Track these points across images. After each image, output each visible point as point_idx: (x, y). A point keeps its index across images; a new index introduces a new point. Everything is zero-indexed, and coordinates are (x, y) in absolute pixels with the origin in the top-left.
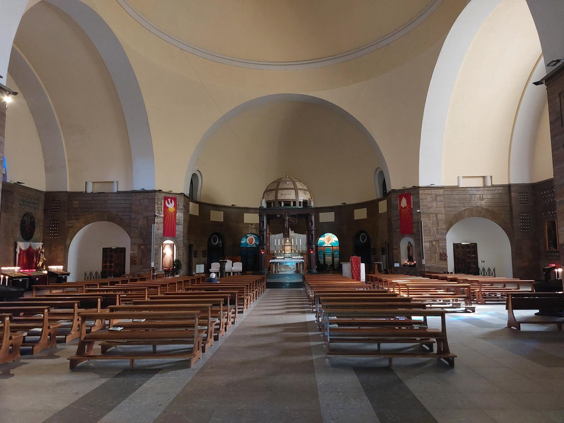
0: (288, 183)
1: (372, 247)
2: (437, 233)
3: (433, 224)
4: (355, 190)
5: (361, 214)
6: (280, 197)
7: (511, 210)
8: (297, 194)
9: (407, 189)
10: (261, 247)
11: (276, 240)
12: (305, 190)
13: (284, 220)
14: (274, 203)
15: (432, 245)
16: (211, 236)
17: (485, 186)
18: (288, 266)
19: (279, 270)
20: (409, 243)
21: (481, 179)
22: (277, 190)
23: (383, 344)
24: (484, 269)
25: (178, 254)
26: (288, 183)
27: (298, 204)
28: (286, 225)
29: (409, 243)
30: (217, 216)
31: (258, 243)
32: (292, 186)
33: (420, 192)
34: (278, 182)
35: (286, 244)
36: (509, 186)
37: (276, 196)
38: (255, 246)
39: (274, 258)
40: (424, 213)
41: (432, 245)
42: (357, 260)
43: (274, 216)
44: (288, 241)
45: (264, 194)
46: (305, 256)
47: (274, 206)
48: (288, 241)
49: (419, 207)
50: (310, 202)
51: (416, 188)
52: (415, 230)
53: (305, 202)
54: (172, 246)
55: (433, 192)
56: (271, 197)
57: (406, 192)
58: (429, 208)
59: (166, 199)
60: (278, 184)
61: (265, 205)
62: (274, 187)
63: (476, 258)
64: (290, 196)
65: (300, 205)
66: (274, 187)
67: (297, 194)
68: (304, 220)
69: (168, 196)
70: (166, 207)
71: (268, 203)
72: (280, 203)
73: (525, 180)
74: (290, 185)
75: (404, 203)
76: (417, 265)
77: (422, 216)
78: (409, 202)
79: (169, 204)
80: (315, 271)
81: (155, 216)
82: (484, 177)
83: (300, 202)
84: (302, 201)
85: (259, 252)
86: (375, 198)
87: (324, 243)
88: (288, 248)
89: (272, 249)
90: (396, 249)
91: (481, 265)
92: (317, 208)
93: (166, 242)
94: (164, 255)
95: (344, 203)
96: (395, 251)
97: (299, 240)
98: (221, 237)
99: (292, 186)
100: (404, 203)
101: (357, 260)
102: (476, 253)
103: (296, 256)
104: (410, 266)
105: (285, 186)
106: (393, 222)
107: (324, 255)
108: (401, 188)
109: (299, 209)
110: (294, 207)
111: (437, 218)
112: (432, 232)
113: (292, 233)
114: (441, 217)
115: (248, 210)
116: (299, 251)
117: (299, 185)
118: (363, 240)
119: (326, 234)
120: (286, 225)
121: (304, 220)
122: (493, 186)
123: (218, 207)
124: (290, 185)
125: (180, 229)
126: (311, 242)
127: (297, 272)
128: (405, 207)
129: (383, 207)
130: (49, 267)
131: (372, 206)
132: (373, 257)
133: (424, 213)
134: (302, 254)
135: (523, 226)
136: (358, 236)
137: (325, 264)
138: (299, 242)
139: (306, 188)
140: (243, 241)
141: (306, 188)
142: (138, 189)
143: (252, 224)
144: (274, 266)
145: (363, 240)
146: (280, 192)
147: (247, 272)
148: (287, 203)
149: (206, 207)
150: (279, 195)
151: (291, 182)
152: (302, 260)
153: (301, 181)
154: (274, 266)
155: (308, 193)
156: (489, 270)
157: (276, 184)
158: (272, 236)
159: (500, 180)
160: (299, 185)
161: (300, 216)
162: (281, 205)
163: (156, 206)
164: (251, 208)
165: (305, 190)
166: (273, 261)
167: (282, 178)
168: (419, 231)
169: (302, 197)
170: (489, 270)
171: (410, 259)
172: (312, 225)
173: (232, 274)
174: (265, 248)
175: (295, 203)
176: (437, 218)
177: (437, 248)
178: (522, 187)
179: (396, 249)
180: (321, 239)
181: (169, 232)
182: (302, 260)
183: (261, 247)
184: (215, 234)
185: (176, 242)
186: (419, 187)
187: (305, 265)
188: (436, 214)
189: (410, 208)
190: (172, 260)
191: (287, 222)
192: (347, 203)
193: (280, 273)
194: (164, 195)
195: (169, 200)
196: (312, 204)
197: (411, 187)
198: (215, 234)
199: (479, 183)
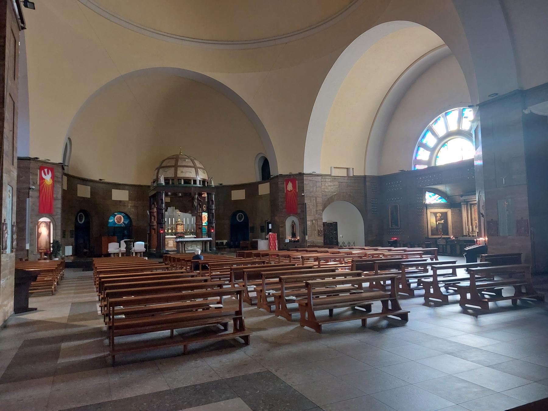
0: (187, 160)
1: (250, 225)
2: (317, 213)
3: (314, 206)
4: (235, 171)
5: (238, 195)
6: (180, 175)
7: (366, 196)
8: (197, 173)
9: (293, 175)
12: (203, 169)
13: (193, 199)
14: (173, 180)
15: (313, 224)
16: (78, 214)
17: (348, 176)
20: (293, 222)
21: (346, 170)
23: (318, 312)
24: (344, 243)
25: (55, 234)
26: (187, 160)
27: (198, 183)
29: (293, 222)
30: (84, 192)
31: (126, 222)
32: (192, 164)
33: (305, 178)
36: (365, 177)
37: (176, 173)
40: (307, 197)
41: (313, 224)
42: (274, 237)
47: (173, 183)
49: (303, 191)
51: (301, 175)
52: (299, 211)
53: (204, 181)
54: (48, 225)
55: (314, 178)
57: (292, 177)
58: (311, 192)
59: (42, 169)
60: (177, 161)
63: (337, 234)
64: (190, 174)
67: (197, 173)
68: (185, 196)
69: (45, 165)
70: (42, 179)
73: (376, 174)
74: (188, 162)
75: (290, 187)
76: (300, 241)
77: (305, 199)
78: (294, 186)
79: (45, 175)
81: (30, 189)
82: (347, 169)
86: (254, 181)
90: (281, 227)
91: (340, 240)
93: (41, 220)
94: (39, 235)
95: (221, 184)
96: (281, 229)
98: (87, 215)
99: (192, 164)
100: (290, 187)
101: (274, 237)
102: (336, 230)
104: (294, 241)
105: (184, 164)
106: (280, 204)
108: (288, 173)
111: (316, 201)
112: (312, 212)
114: (319, 200)
115: (118, 186)
118: (240, 219)
121: (185, 196)
122: (354, 176)
123: (85, 181)
124: (188, 162)
125: (58, 205)
128: (291, 191)
129: (264, 189)
131: (251, 189)
132: (250, 235)
133: (307, 197)
135: (373, 208)
136: (234, 215)
138: (191, 221)
140: (110, 221)
142: (32, 156)
145: (240, 219)
146: (180, 170)
148: (187, 181)
149: (74, 181)
150: (179, 172)
151: (189, 160)
156: (349, 243)
159: (358, 172)
163: (31, 177)
168: (304, 212)
169: (201, 176)
170: (349, 243)
171: (294, 235)
173: (120, 256)
175: (195, 182)
176: (316, 201)
177: (316, 226)
178: (373, 177)
179: (281, 227)
181: (45, 209)
184: (81, 211)
185: (53, 220)
186: (304, 174)
188: (316, 198)
189: (296, 191)
190: (48, 240)
192: (224, 184)
194: (40, 164)
195: (46, 170)
196: (213, 184)
197: (297, 173)
198: (81, 211)
199: (343, 173)
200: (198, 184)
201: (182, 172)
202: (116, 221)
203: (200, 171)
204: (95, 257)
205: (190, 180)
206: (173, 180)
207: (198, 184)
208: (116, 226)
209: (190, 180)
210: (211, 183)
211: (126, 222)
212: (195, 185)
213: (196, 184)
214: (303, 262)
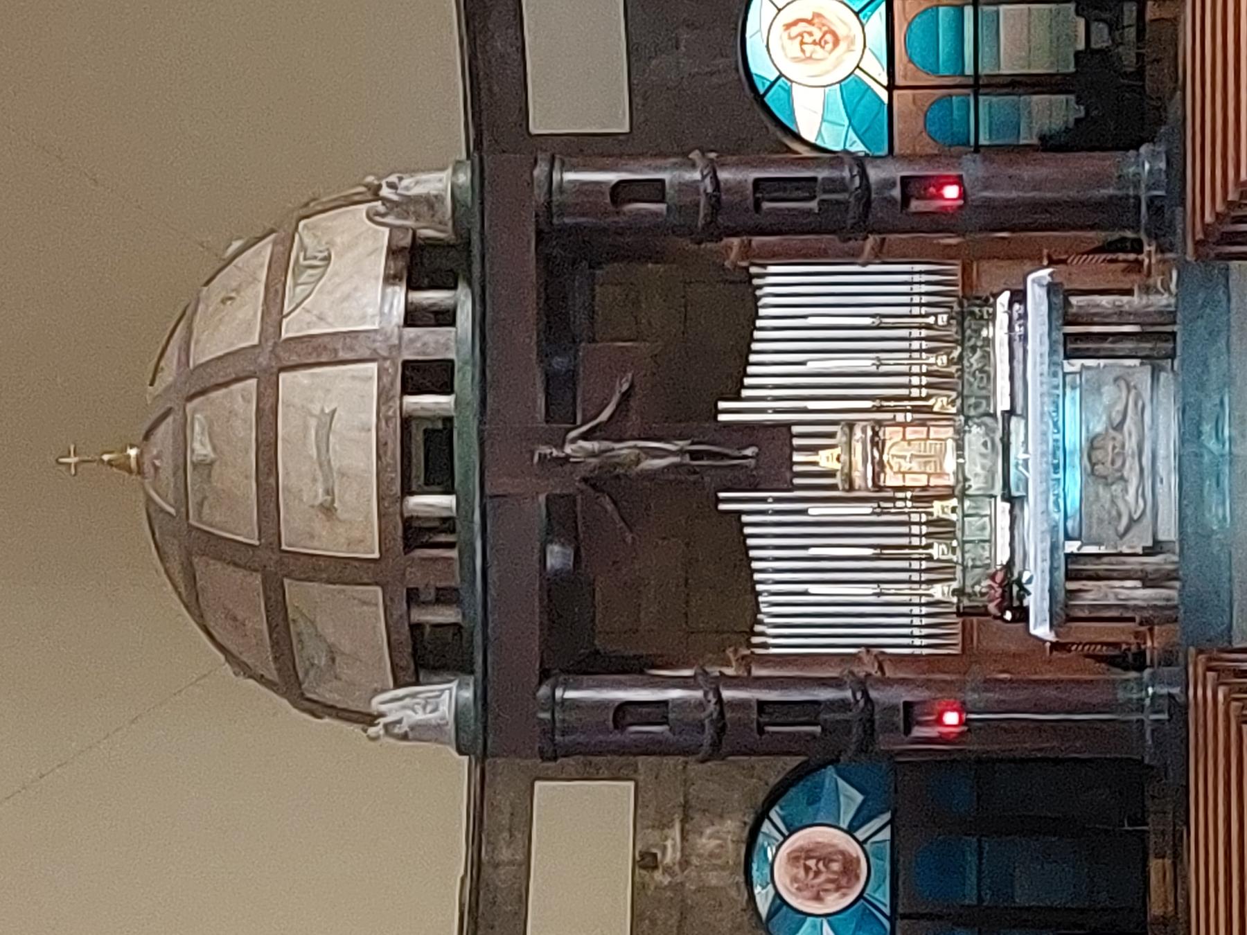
0: (201, 448)
6: (358, 530)
8: (322, 352)
10: (884, 742)
11: (819, 591)
12: (280, 268)
13: (606, 480)
14: (413, 597)
18: (1093, 445)
19: (1139, 540)
22: (278, 568)
28: (660, 456)
31: (851, 798)
34: (191, 553)
35: (862, 474)
37: (342, 571)
38: (878, 830)
39: (1010, 590)
43: (561, 596)
44: (826, 460)
45: (319, 709)
46: (990, 274)
47: (444, 597)
48: (826, 460)
50: (406, 205)
53: (416, 264)
56: (354, 625)
61: (444, 699)
62: (240, 590)
64: (340, 425)
65: (445, 317)
66: (244, 589)
67: (322, 352)
71: (423, 657)
72: (416, 533)
74: (219, 429)
80: (1146, 163)
83: (413, 317)
84: (398, 297)
85: (946, 761)
87: (852, 89)
88: (911, 457)
89: (910, 636)
92: (477, 145)
97: (815, 336)
103: (986, 374)
105: (239, 476)
107: (978, 85)
109: (480, 322)
110: (465, 379)
113: (754, 405)
116: (937, 343)
117: (229, 327)
119: (760, 66)
120: (660, 456)
124: (219, 429)
126: (843, 214)
127: (1155, 342)
130: (730, 413)
134: (970, 309)
137: (1088, 77)
139: (265, 249)
141: (265, 249)
143: (646, 861)
144: (1094, 593)
146: (302, 531)
147: (1155, 909)
148: (424, 453)
150: (329, 542)
151: (199, 414)
152: (1036, 297)
153: (186, 315)
154: (1094, 593)
155: (308, 235)
157: (218, 578)
158: (777, 631)
160: (229, 327)
161: (556, 325)
162: (447, 523)
164: (476, 866)
165: (280, 268)
166: (1037, 602)
167: (152, 513)
169: (354, 289)
172: (656, 190)
174: (901, 695)
175: (423, 375)
180: (816, 117)
182: (1036, 297)
183: (884, 742)
187: (1095, 270)
191: (624, 449)
193: (1168, 531)
196: (436, 183)
200: (453, 342)
201: (328, 510)
202: (834, 902)
203: (314, 311)
204: (1145, 914)
205: (407, 422)
206: (413, 597)
207: (453, 342)
208: (882, 897)
209: (407, 422)
210: (430, 202)
211: (851, 798)
212: (465, 379)
213: (447, 367)
214: (1051, 105)
